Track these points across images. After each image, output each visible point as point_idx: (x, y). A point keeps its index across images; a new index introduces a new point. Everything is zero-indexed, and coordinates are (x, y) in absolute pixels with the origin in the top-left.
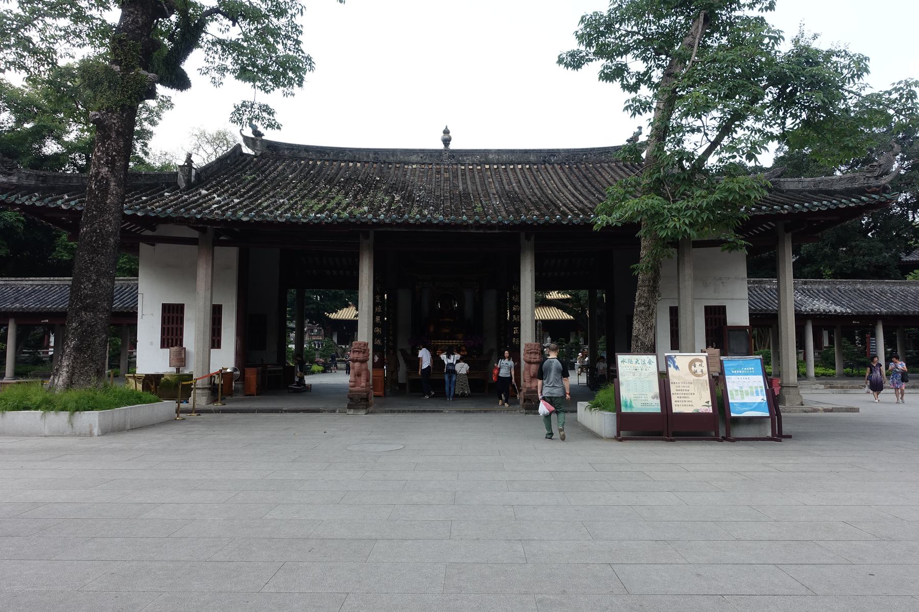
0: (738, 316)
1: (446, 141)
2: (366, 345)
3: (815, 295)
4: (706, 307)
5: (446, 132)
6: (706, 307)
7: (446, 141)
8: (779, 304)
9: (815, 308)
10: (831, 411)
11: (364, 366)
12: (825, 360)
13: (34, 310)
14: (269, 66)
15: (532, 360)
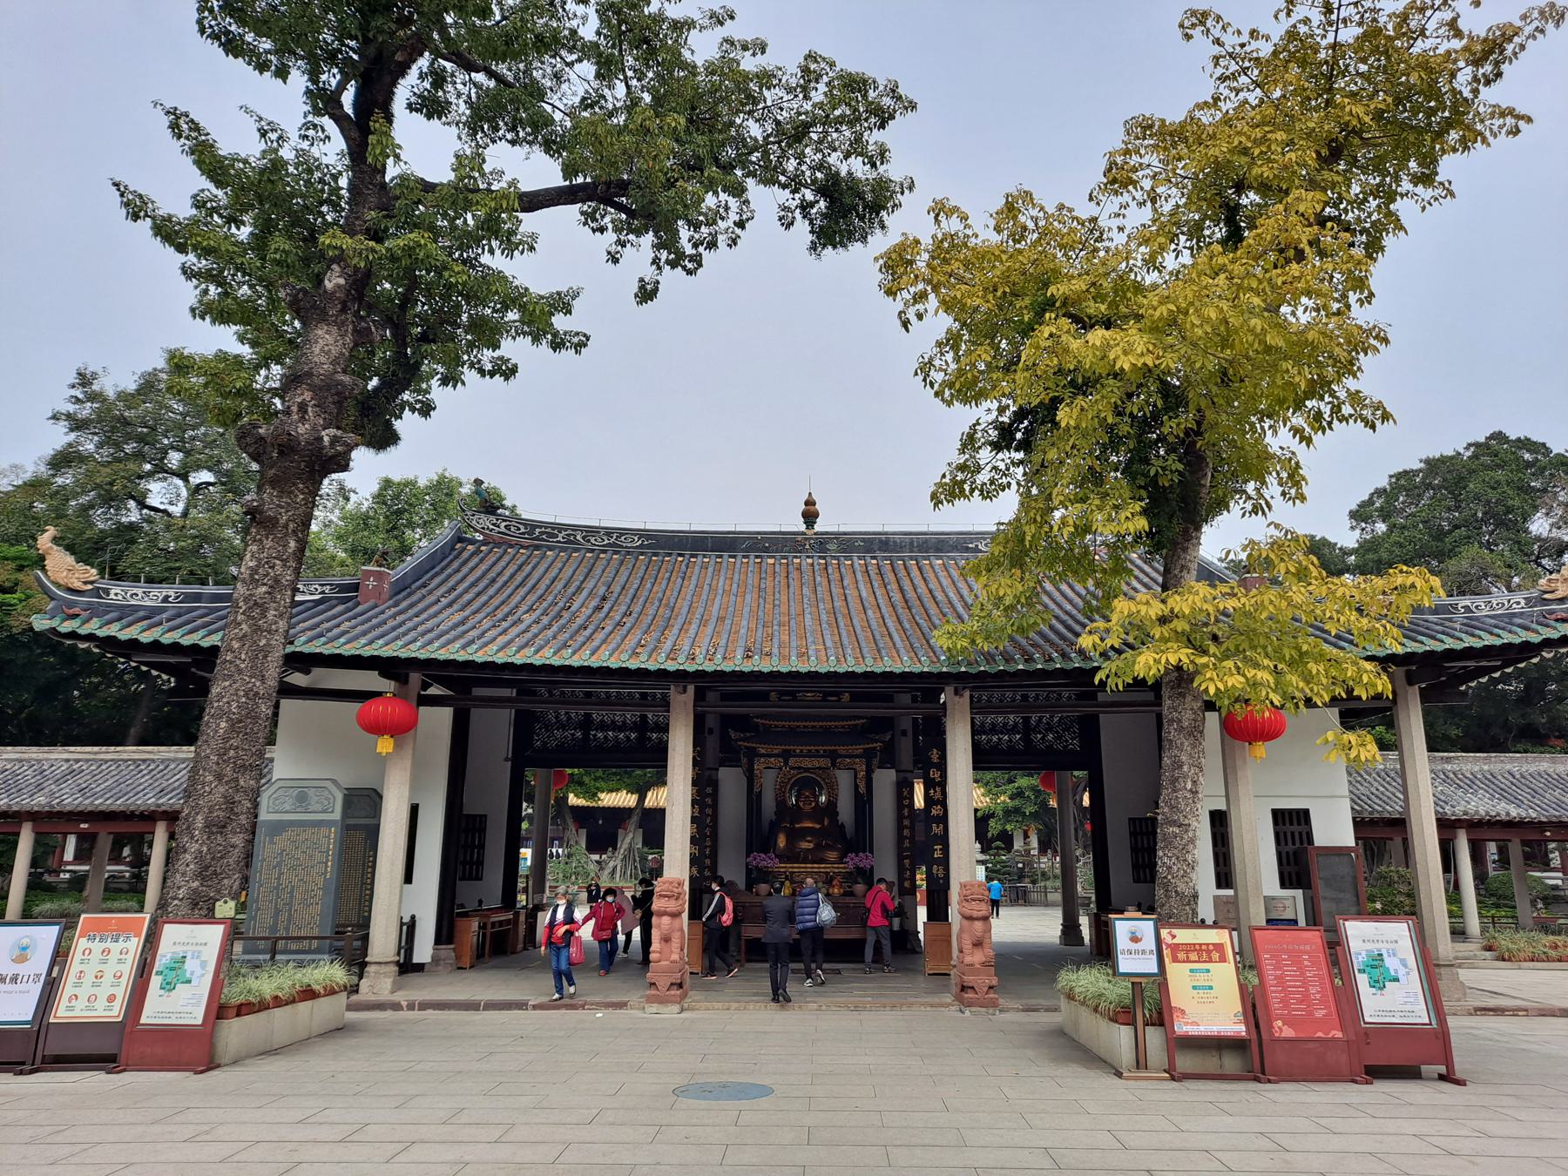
0: (1334, 828)
1: (810, 516)
2: (680, 884)
3: (1471, 783)
4: (1275, 813)
5: (810, 503)
6: (1275, 813)
7: (810, 516)
8: (1406, 800)
9: (1472, 807)
10: (1498, 1011)
11: (677, 922)
12: (1493, 897)
13: (68, 808)
14: (276, 52)
15: (975, 914)
